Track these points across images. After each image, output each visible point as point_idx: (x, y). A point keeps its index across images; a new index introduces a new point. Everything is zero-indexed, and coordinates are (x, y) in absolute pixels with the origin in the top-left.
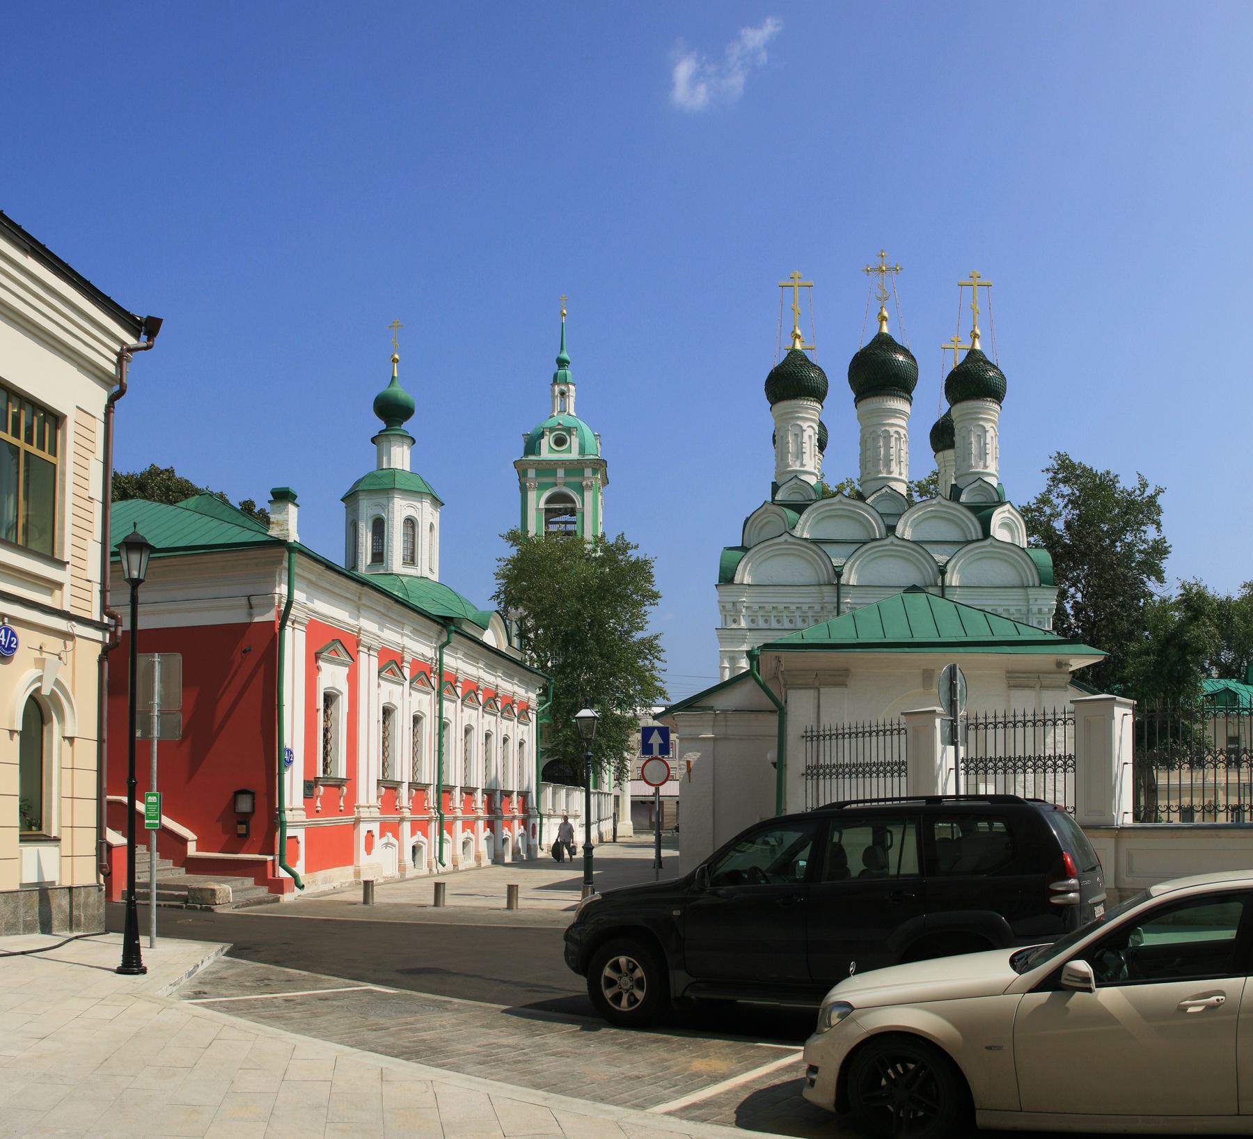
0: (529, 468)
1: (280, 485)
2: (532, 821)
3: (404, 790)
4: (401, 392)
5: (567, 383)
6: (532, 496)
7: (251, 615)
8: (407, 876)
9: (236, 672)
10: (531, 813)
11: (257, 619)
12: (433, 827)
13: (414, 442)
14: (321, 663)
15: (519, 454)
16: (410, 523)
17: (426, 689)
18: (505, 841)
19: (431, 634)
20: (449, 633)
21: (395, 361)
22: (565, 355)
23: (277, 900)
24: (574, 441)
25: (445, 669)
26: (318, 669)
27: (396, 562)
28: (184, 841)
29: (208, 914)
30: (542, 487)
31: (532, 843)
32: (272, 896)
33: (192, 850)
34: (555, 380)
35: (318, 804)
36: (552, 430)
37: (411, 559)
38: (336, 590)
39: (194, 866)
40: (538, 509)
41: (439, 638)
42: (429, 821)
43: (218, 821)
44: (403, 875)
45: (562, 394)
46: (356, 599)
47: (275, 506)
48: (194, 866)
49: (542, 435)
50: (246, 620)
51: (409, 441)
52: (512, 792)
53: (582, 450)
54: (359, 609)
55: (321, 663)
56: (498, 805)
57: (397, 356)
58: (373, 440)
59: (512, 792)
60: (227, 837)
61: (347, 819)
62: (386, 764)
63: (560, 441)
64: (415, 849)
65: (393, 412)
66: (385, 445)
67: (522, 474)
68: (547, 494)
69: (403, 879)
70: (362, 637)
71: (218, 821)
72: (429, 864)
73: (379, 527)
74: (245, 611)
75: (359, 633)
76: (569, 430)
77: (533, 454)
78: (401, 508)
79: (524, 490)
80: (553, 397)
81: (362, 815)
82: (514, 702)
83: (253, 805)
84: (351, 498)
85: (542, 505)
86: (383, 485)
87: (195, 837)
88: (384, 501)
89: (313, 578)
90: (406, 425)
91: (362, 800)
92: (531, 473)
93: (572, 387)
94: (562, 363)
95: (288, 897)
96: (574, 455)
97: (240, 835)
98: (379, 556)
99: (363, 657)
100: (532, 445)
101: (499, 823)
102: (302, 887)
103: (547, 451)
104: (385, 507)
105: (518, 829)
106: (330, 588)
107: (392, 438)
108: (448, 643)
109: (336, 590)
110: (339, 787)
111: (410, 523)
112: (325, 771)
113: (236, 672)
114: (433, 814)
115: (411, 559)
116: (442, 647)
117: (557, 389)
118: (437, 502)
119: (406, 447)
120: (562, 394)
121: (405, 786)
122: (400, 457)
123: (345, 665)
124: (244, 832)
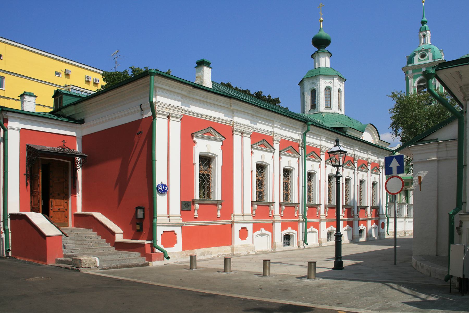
0: (408, 67)
1: (199, 59)
2: (381, 221)
3: (369, 210)
4: (324, 34)
5: (426, 31)
6: (411, 82)
7: (142, 115)
8: (276, 250)
9: (137, 145)
10: (381, 217)
11: (145, 116)
12: (301, 226)
13: (331, 55)
14: (195, 139)
15: (404, 64)
16: (328, 89)
17: (316, 160)
18: (361, 231)
19: (297, 127)
20: (309, 125)
21: (321, 21)
22: (425, 19)
23: (148, 265)
24: (430, 55)
25: (307, 144)
26: (195, 142)
27: (322, 107)
28: (113, 234)
29: (77, 274)
30: (415, 77)
31: (381, 231)
32: (147, 262)
33: (119, 238)
34: (420, 30)
35: (219, 213)
36: (419, 52)
37: (329, 105)
38: (208, 101)
39: (120, 246)
40: (414, 87)
41: (303, 129)
42: (298, 222)
43: (130, 224)
44: (274, 250)
45: (424, 36)
46: (229, 107)
47: (198, 69)
48: (120, 246)
49: (415, 55)
50: (140, 118)
51: (328, 54)
52: (367, 207)
53: (434, 57)
54: (232, 112)
55: (195, 139)
56: (356, 213)
57: (322, 19)
58: (312, 57)
59: (367, 207)
60: (134, 231)
61: (228, 222)
62: (286, 196)
63: (423, 56)
64: (287, 237)
65: (321, 43)
66: (317, 58)
67: (406, 73)
68: (418, 80)
69: (274, 252)
70: (235, 127)
71: (130, 224)
72: (298, 244)
73: (314, 93)
74: (139, 113)
75: (233, 125)
76: (427, 50)
77: (411, 63)
78: (323, 83)
79: (407, 79)
80: (420, 38)
81: (276, 219)
82: (368, 163)
83: (144, 214)
84: (301, 83)
85: (416, 85)
86: (315, 75)
87: (122, 231)
88: (315, 82)
89: (184, 93)
90: (328, 48)
91: (237, 209)
92: (410, 72)
93: (428, 32)
94: (423, 23)
95: (155, 264)
96: (430, 60)
97: (138, 230)
98: (314, 106)
99: (237, 138)
100: (410, 60)
101: (356, 223)
102: (168, 258)
103: (417, 61)
104: (316, 84)
105: (370, 225)
106: (203, 99)
107: (319, 54)
108: (308, 131)
109: (208, 101)
110: (216, 205)
111: (328, 89)
112: (360, 204)
113: (137, 145)
114: (301, 218)
115: (329, 105)
116: (305, 133)
117: (421, 34)
118: (341, 79)
119: (327, 57)
120: (424, 36)
121: (369, 208)
122: (324, 62)
123: (219, 141)
124: (139, 229)
